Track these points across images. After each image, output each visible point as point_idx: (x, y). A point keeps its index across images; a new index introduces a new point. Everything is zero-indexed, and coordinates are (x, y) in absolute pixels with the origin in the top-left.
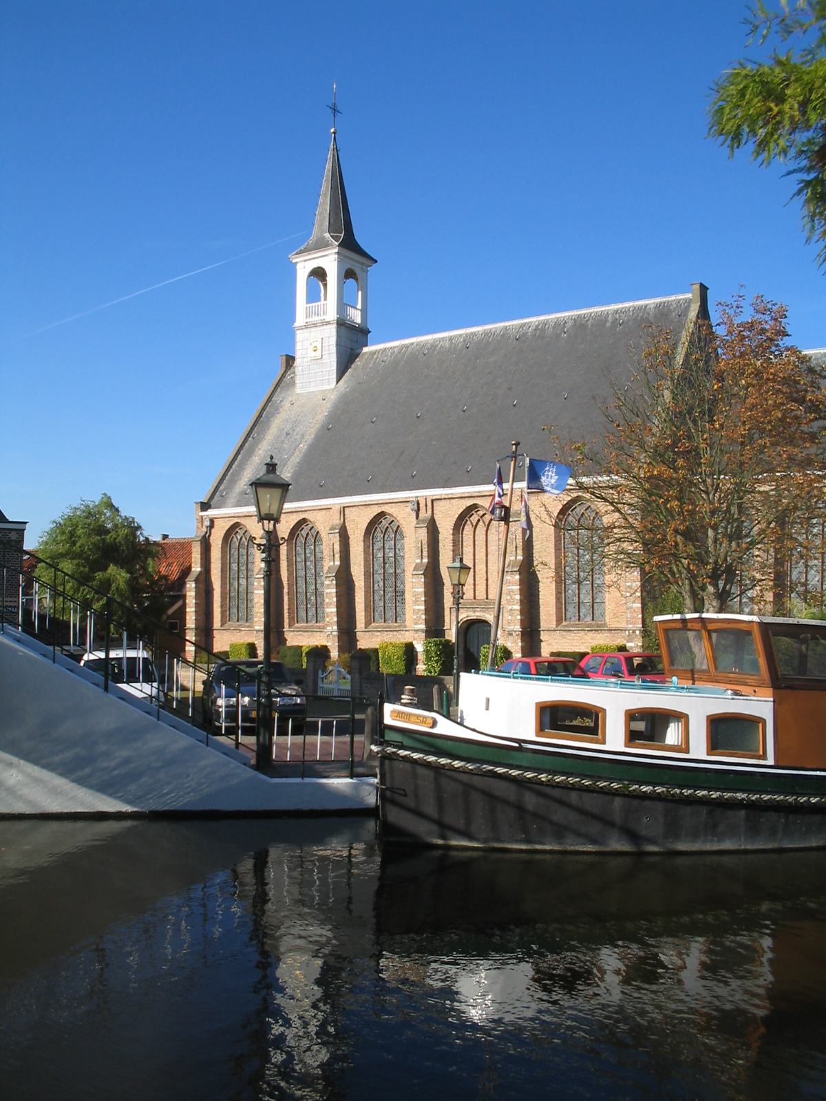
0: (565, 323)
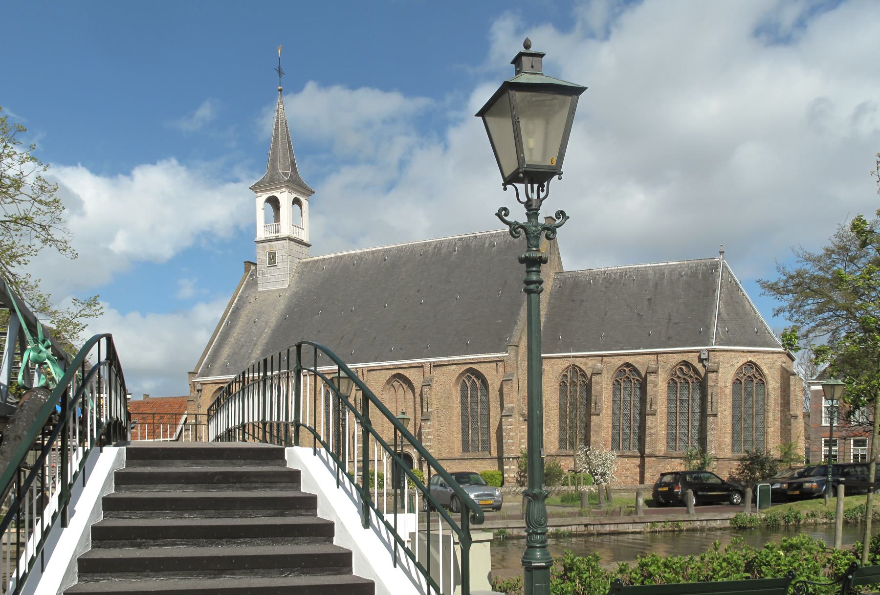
0: (456, 244)
